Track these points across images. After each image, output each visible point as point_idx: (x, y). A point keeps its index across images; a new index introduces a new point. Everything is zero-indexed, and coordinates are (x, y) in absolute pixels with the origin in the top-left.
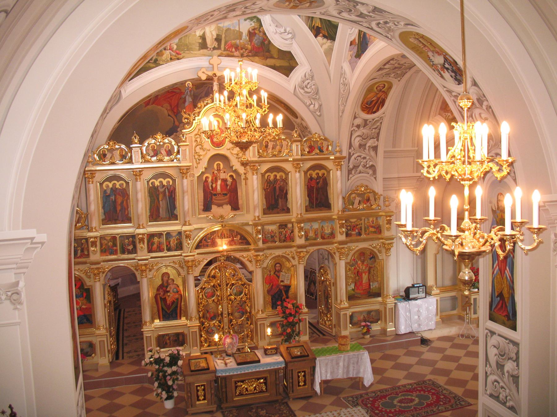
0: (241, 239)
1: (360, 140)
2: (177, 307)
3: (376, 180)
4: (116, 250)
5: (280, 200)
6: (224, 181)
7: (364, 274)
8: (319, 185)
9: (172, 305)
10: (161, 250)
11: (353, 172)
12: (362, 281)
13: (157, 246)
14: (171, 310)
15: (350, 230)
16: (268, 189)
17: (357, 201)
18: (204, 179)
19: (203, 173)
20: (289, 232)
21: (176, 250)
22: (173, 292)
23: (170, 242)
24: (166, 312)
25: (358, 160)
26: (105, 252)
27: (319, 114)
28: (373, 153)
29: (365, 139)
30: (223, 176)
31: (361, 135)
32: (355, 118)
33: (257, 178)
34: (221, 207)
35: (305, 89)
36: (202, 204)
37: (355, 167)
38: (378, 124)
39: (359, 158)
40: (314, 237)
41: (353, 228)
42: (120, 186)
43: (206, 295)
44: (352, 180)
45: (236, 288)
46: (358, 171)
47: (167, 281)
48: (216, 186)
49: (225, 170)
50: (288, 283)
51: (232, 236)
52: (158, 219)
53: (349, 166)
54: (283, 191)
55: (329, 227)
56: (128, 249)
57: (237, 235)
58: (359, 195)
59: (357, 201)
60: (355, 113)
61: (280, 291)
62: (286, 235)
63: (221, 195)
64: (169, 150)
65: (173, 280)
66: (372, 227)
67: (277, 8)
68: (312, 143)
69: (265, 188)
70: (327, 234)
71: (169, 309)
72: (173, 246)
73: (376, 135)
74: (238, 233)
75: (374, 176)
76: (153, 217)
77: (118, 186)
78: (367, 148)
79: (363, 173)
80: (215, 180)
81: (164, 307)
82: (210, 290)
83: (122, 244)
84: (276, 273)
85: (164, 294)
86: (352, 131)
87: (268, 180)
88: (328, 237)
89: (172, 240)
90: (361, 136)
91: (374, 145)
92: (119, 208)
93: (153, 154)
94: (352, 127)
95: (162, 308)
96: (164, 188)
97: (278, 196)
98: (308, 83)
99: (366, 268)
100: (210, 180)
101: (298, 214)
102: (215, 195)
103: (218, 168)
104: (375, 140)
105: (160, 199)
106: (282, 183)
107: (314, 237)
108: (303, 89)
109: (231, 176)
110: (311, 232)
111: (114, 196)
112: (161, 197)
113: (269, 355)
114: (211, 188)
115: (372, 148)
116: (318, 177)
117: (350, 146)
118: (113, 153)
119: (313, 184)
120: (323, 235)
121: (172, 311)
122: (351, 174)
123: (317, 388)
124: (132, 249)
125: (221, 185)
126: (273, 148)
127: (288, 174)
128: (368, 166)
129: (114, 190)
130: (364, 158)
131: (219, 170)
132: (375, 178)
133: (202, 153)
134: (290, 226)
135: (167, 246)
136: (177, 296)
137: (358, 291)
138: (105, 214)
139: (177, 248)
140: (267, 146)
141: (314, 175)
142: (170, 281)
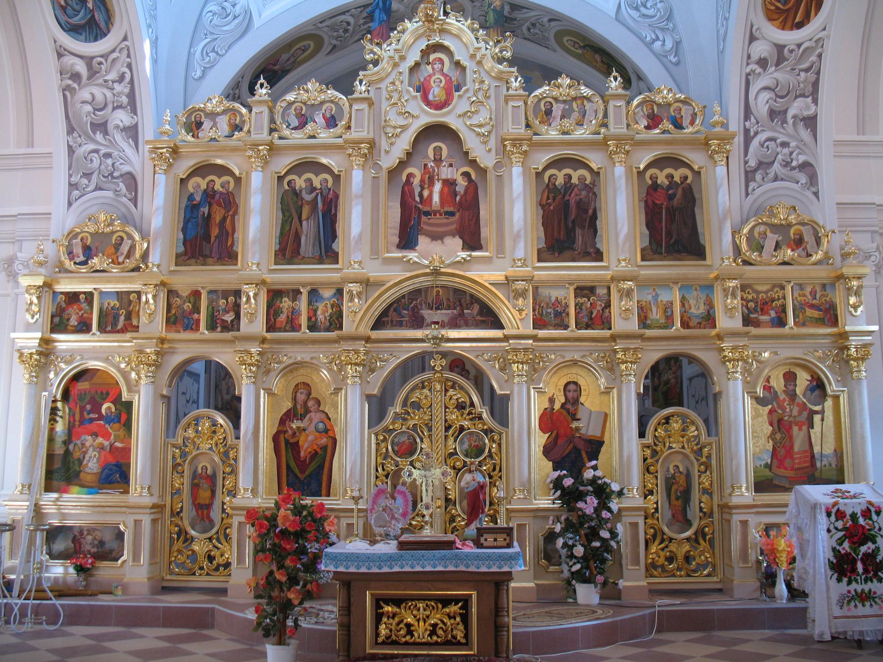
0: (481, 313)
1: (771, 98)
2: (321, 467)
3: (818, 198)
5: (578, 232)
6: (449, 184)
7: (795, 429)
8: (675, 202)
9: (310, 463)
10: (295, 328)
11: (758, 177)
12: (792, 447)
13: (288, 317)
14: (308, 472)
15: (755, 311)
17: (770, 244)
18: (404, 178)
19: (402, 164)
20: (600, 305)
21: (328, 330)
22: (317, 430)
23: (315, 311)
24: (296, 476)
25: (768, 147)
26: (175, 323)
27: (674, 60)
28: (805, 134)
29: (782, 97)
30: (446, 172)
31: (773, 87)
32: (752, 39)
34: (439, 241)
35: (642, 9)
36: (398, 232)
37: (764, 165)
38: (813, 58)
39: (771, 144)
40: (663, 321)
41: (764, 306)
42: (223, 187)
43: (396, 448)
44: (755, 196)
45: (469, 440)
46: (771, 175)
47: (305, 403)
48: (430, 196)
49: (452, 161)
50: (598, 434)
51: (461, 305)
52: (296, 260)
53: (746, 163)
54: (588, 210)
55: (702, 301)
56: (223, 321)
57: (472, 303)
58: (775, 228)
59: (770, 244)
60: (752, 26)
61: (577, 451)
62: (592, 313)
63: (441, 215)
64: (333, 117)
65: (319, 403)
66: (812, 306)
68: (655, 108)
70: (697, 317)
71: (302, 471)
72: (323, 320)
73: (810, 88)
75: (814, 189)
76: (284, 255)
77: (217, 187)
78: (790, 121)
79: (782, 180)
80: (429, 179)
81: (293, 464)
82: (404, 438)
83: (213, 308)
86: (748, 75)
88: (700, 323)
89: (321, 306)
90: (773, 90)
91: (806, 113)
92: (215, 232)
93: (297, 124)
94: (748, 64)
95: (288, 467)
96: (314, 194)
97: (573, 222)
99: (800, 413)
100: (416, 181)
102: (427, 214)
103: (438, 157)
104: (809, 100)
107: (663, 321)
108: (637, 9)
109: (466, 175)
110: (654, 309)
111: (207, 207)
114: (418, 199)
115: (801, 120)
116: (670, 183)
117: (748, 112)
119: (660, 199)
120: (685, 318)
121: (310, 476)
122: (754, 180)
124: (232, 321)
125: (442, 193)
126: (563, 117)
128: (794, 164)
129: (209, 195)
130: (784, 145)
131: (438, 160)
132: (816, 194)
134: (602, 291)
135: (309, 319)
136: (324, 441)
137: (782, 471)
138: (184, 243)
139: (331, 324)
141: (662, 179)
142: (310, 403)
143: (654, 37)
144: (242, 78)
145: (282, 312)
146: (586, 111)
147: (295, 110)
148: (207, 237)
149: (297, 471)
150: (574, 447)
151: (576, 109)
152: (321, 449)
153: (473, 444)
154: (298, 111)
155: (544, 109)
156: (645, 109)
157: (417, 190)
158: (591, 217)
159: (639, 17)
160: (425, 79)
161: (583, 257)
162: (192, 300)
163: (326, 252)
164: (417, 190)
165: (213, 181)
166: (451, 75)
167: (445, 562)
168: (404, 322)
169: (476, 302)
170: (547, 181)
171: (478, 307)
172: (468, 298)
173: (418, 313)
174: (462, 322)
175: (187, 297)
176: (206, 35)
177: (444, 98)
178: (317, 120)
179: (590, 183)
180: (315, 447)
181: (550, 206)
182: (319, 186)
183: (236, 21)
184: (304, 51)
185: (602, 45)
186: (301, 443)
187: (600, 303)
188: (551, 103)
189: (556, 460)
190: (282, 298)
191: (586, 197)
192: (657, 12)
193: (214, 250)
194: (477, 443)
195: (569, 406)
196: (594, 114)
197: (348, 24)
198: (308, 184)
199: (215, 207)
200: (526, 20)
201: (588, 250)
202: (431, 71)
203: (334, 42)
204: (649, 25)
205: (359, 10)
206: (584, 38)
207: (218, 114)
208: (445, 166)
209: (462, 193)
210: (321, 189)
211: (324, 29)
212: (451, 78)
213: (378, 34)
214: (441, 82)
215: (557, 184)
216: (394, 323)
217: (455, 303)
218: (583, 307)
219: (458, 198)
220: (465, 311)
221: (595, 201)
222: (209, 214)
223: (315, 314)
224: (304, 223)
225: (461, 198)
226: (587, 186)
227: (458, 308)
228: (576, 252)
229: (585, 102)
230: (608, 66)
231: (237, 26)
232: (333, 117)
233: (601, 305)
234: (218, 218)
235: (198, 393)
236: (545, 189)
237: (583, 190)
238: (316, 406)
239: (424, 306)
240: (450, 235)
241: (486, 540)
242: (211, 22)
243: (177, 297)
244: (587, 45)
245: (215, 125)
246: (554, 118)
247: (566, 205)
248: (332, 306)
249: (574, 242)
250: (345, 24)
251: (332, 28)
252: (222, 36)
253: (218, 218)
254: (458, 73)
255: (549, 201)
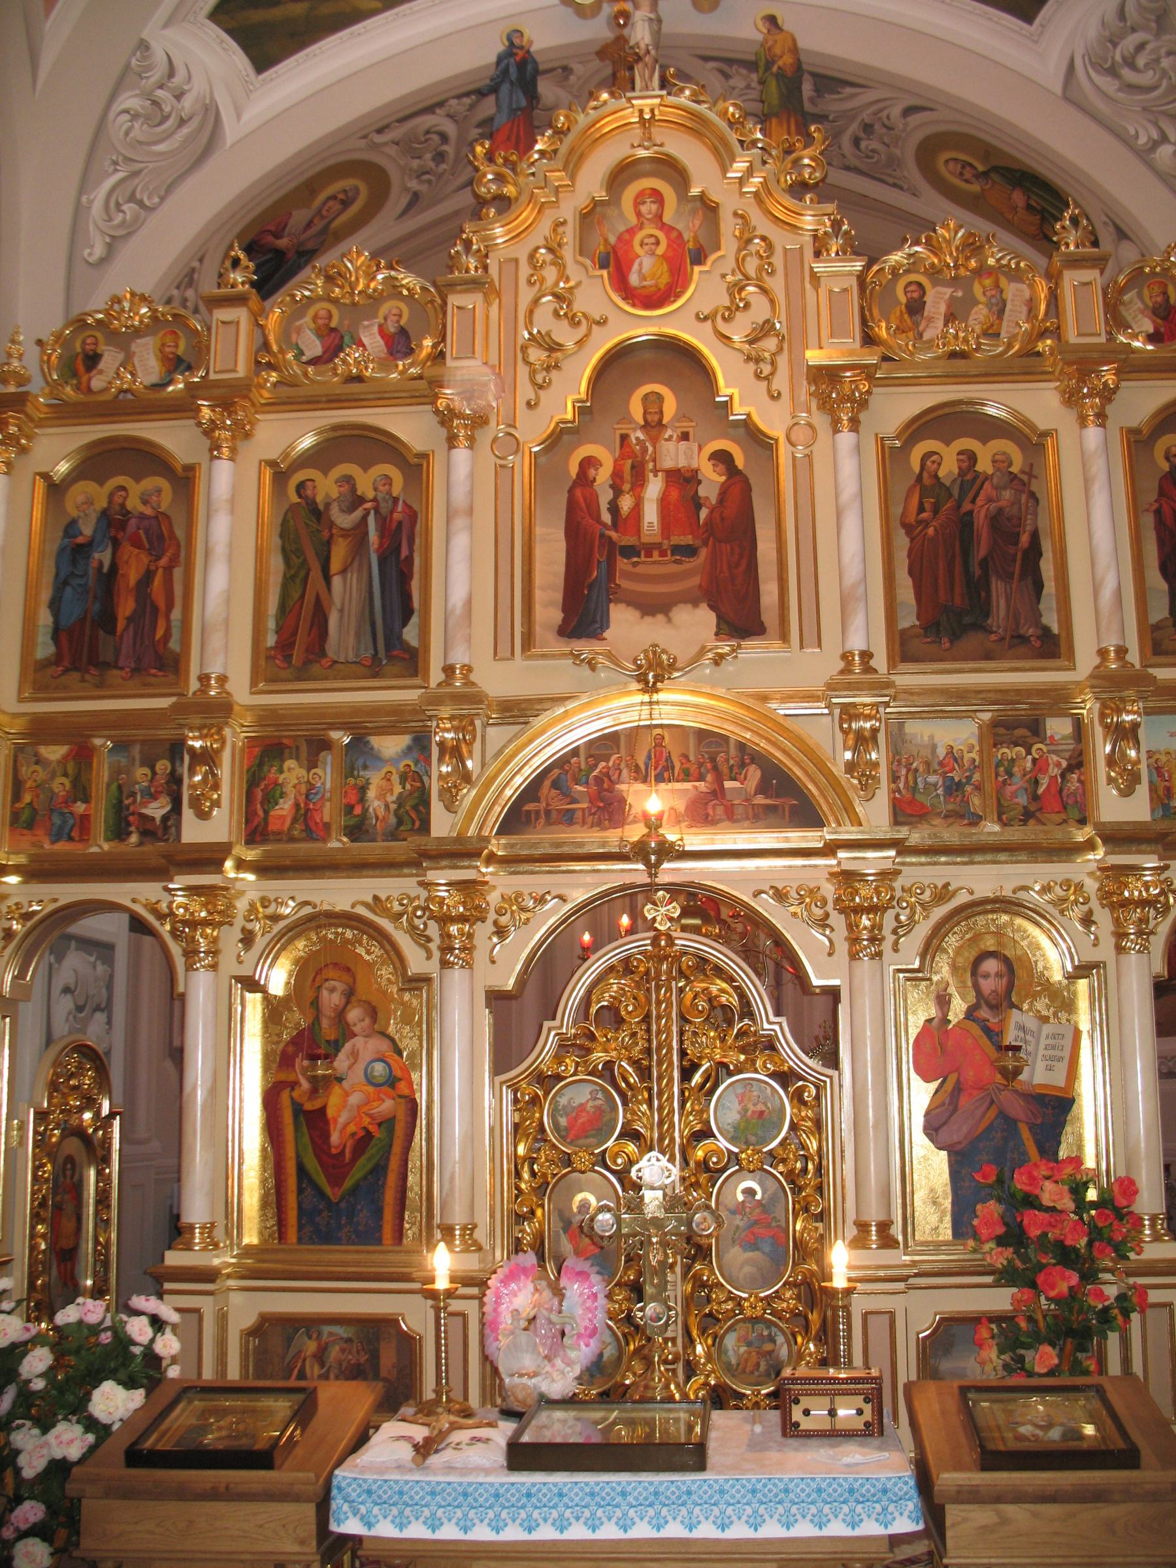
0: (763, 788)
2: (379, 1170)
4: (84, 821)
5: (997, 587)
9: (355, 1159)
13: (297, 805)
14: (349, 1183)
16: (926, 524)
18: (574, 469)
20: (1056, 764)
21: (393, 836)
22: (370, 1080)
23: (363, 789)
26: (30, 825)
30: (673, 454)
33: (858, 448)
34: (660, 617)
35: (1126, 73)
36: (559, 596)
42: (145, 502)
43: (563, 1121)
47: (341, 1014)
49: (686, 426)
50: (1058, 1079)
51: (715, 768)
54: (1017, 536)
57: (743, 765)
62: (1037, 783)
63: (663, 554)
64: (403, 331)
67: (1047, 567)
69: (912, 518)
71: (335, 1181)
72: (381, 812)
74: (747, 755)
76: (288, 658)
77: (133, 503)
81: (312, 1164)
83: (120, 787)
84: (984, 1013)
85: (314, 1092)
87: (927, 480)
89: (375, 779)
92: (126, 607)
95: (301, 1170)
96: (358, 513)
97: (984, 564)
98: (1141, 47)
100: (603, 476)
101: (1103, 653)
102: (629, 552)
105: (335, 565)
106: (1007, 494)
109: (722, 458)
112: (339, 553)
113: (809, 1435)
114: (606, 517)
118: (134, 347)
121: (354, 1191)
123: (575, 1210)
124: (165, 818)
125: (664, 503)
126: (950, 318)
127: (1040, 448)
131: (654, 426)
133: (566, 336)
136: (387, 1106)
139: (400, 822)
140: (916, 308)
143: (1155, 135)
144: (201, 260)
145: (283, 795)
146: (1004, 303)
147: (315, 318)
148: (107, 620)
149: (321, 1180)
150: (1002, 1115)
151: (982, 299)
152: (380, 1125)
153: (751, 1108)
154: (321, 322)
155: (903, 300)
156: (1146, 292)
157: (605, 497)
158: (1026, 553)
159: (1119, 90)
160: (620, 238)
161: (1010, 647)
162: (70, 770)
163: (389, 647)
164: (605, 497)
165: (123, 488)
166: (680, 226)
167: (690, 1513)
168: (579, 814)
169: (753, 761)
170: (916, 467)
171: (758, 774)
172: (733, 751)
173: (611, 790)
174: (720, 810)
175: (59, 762)
176: (115, 163)
177: (664, 280)
178: (365, 341)
179: (1023, 472)
180: (366, 1121)
181: (927, 526)
182: (370, 494)
183: (185, 131)
184: (346, 204)
185: (1034, 165)
186: (330, 1113)
187: (1055, 758)
188: (920, 285)
189: (958, 1147)
190: (283, 761)
191: (1013, 504)
192: (1161, 79)
193: (124, 650)
194: (760, 1107)
195: (984, 1013)
196: (1025, 309)
197: (444, 138)
198: (345, 488)
199: (127, 550)
200: (850, 116)
201: (1022, 632)
202: (633, 220)
203: (414, 184)
204: (1145, 109)
205: (467, 101)
206: (987, 151)
207: (137, 333)
208: (670, 439)
209: (714, 501)
210: (375, 500)
211: (387, 150)
212: (680, 235)
213: (508, 139)
214: (658, 243)
215: (941, 474)
216: (554, 815)
217: (701, 765)
218: (1016, 769)
219: (704, 514)
220: (728, 784)
221: (1035, 514)
222: (114, 567)
223: (362, 799)
224: (337, 581)
225: (711, 512)
226: (1013, 477)
227: (709, 777)
228: (993, 637)
229: (1003, 282)
230: (1043, 219)
231: (187, 141)
232: (403, 331)
233: (1058, 765)
234: (133, 575)
235: (110, 987)
236: (914, 486)
237: (1005, 488)
238: (367, 1021)
239: (625, 772)
240: (685, 602)
241: (806, 1412)
242: (127, 134)
243: (37, 763)
244: (995, 169)
245: (127, 362)
246: (930, 320)
247: (966, 523)
248: (403, 778)
249: (987, 615)
250: (436, 138)
251: (408, 146)
252: (151, 165)
253: (133, 575)
254: (697, 223)
255: (924, 515)
